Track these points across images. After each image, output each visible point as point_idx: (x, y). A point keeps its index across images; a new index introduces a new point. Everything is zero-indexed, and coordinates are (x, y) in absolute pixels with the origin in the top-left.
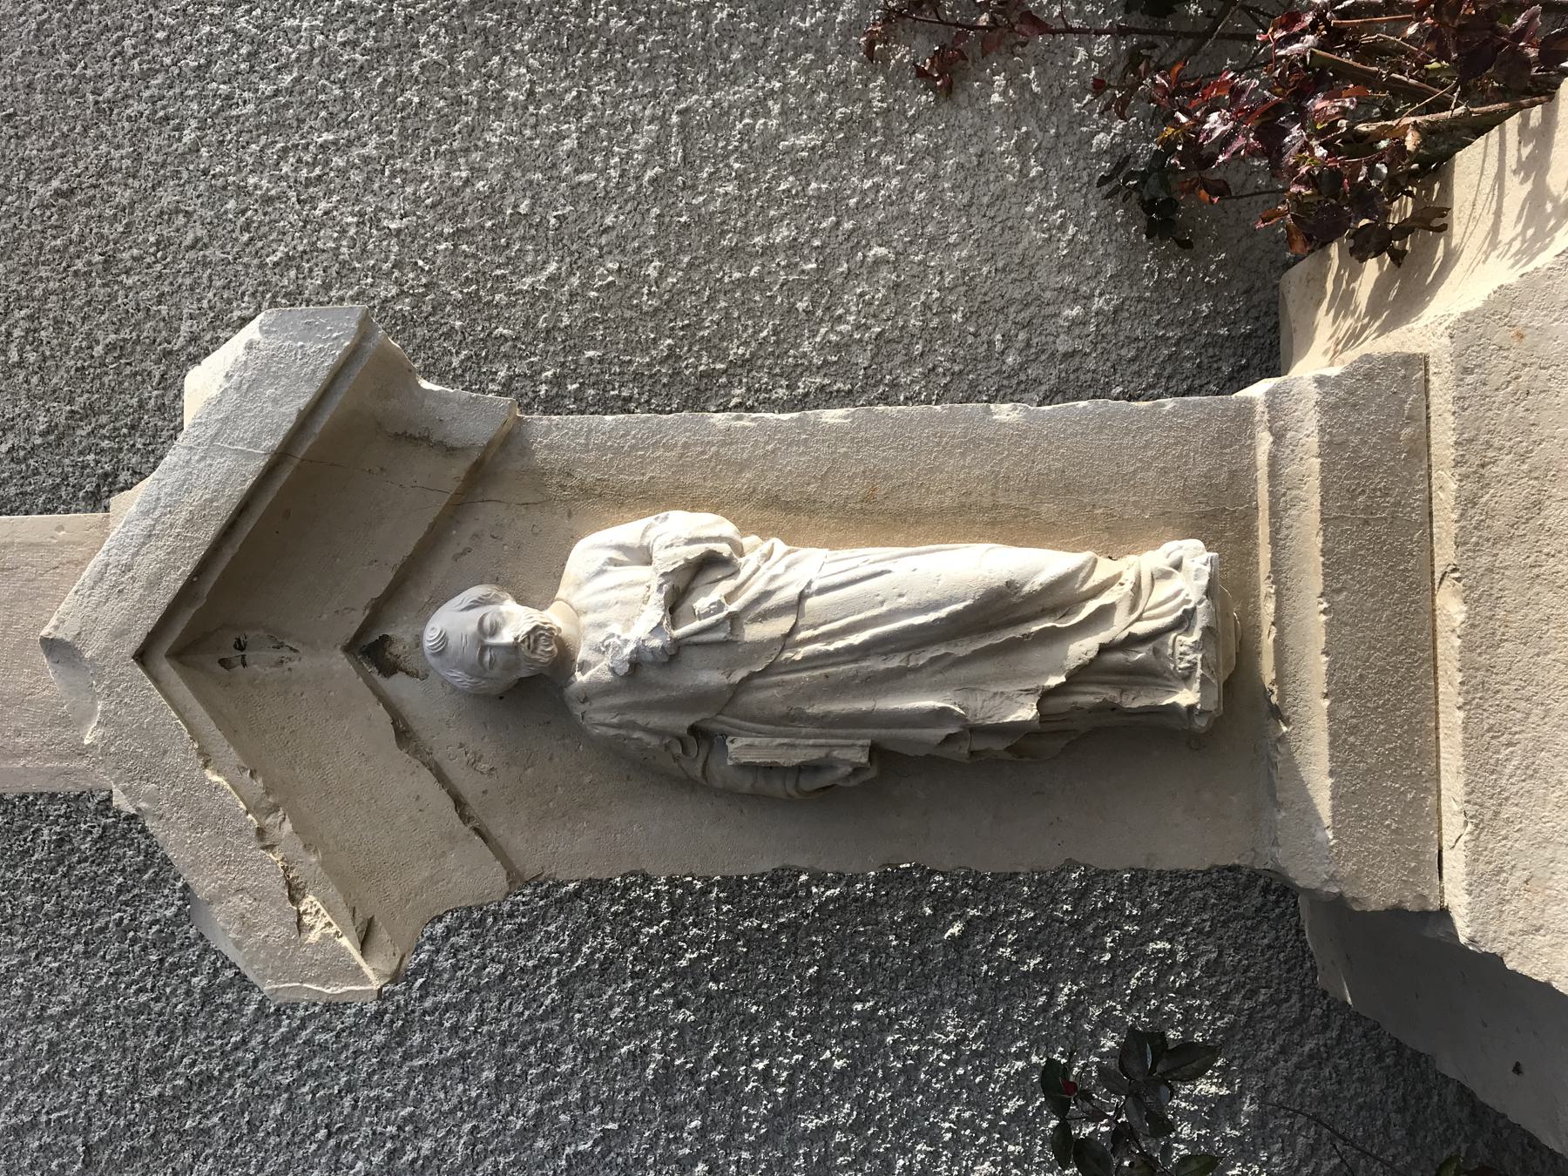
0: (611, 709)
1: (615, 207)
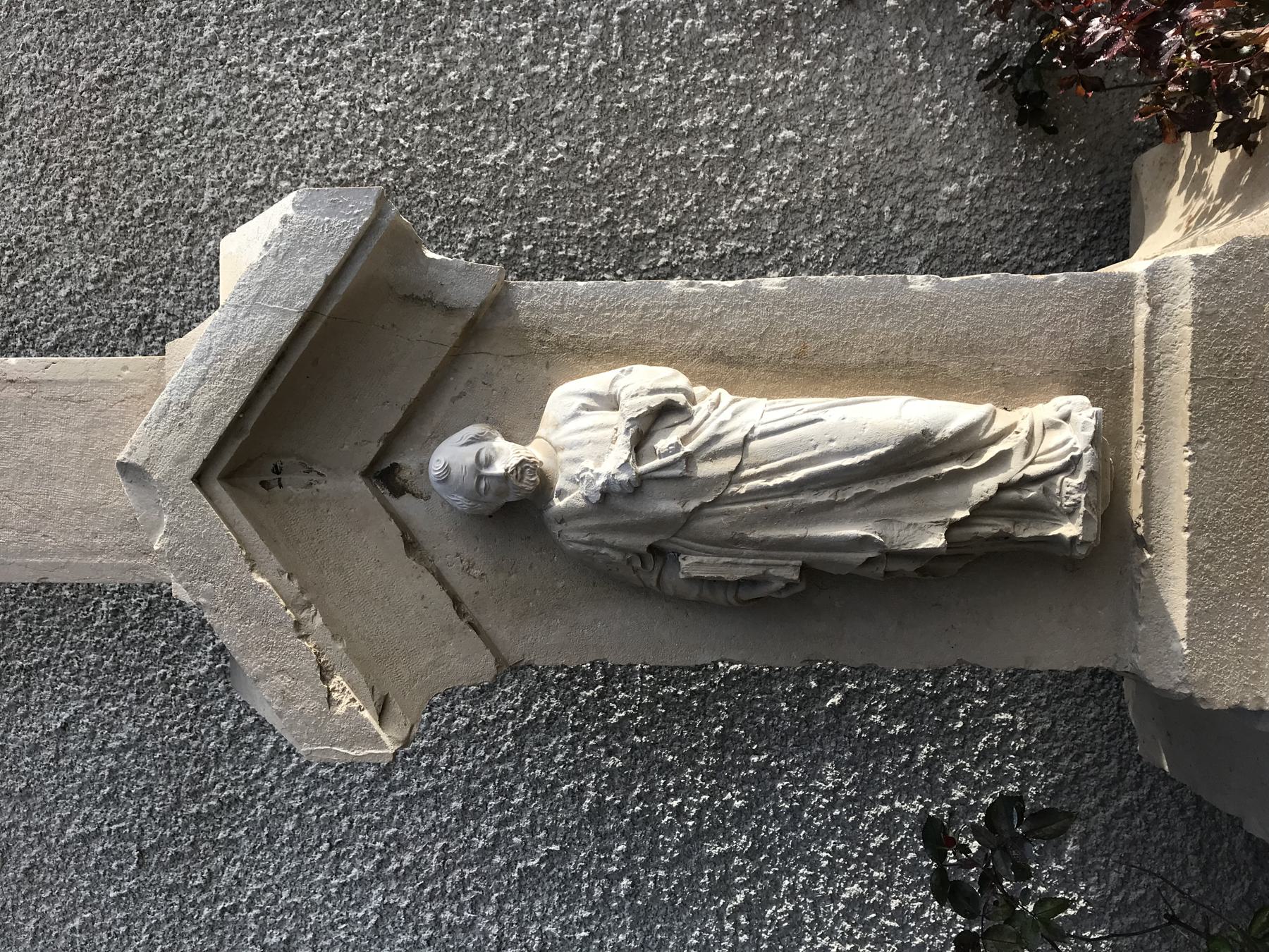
0: (582, 530)
1: (565, 94)
